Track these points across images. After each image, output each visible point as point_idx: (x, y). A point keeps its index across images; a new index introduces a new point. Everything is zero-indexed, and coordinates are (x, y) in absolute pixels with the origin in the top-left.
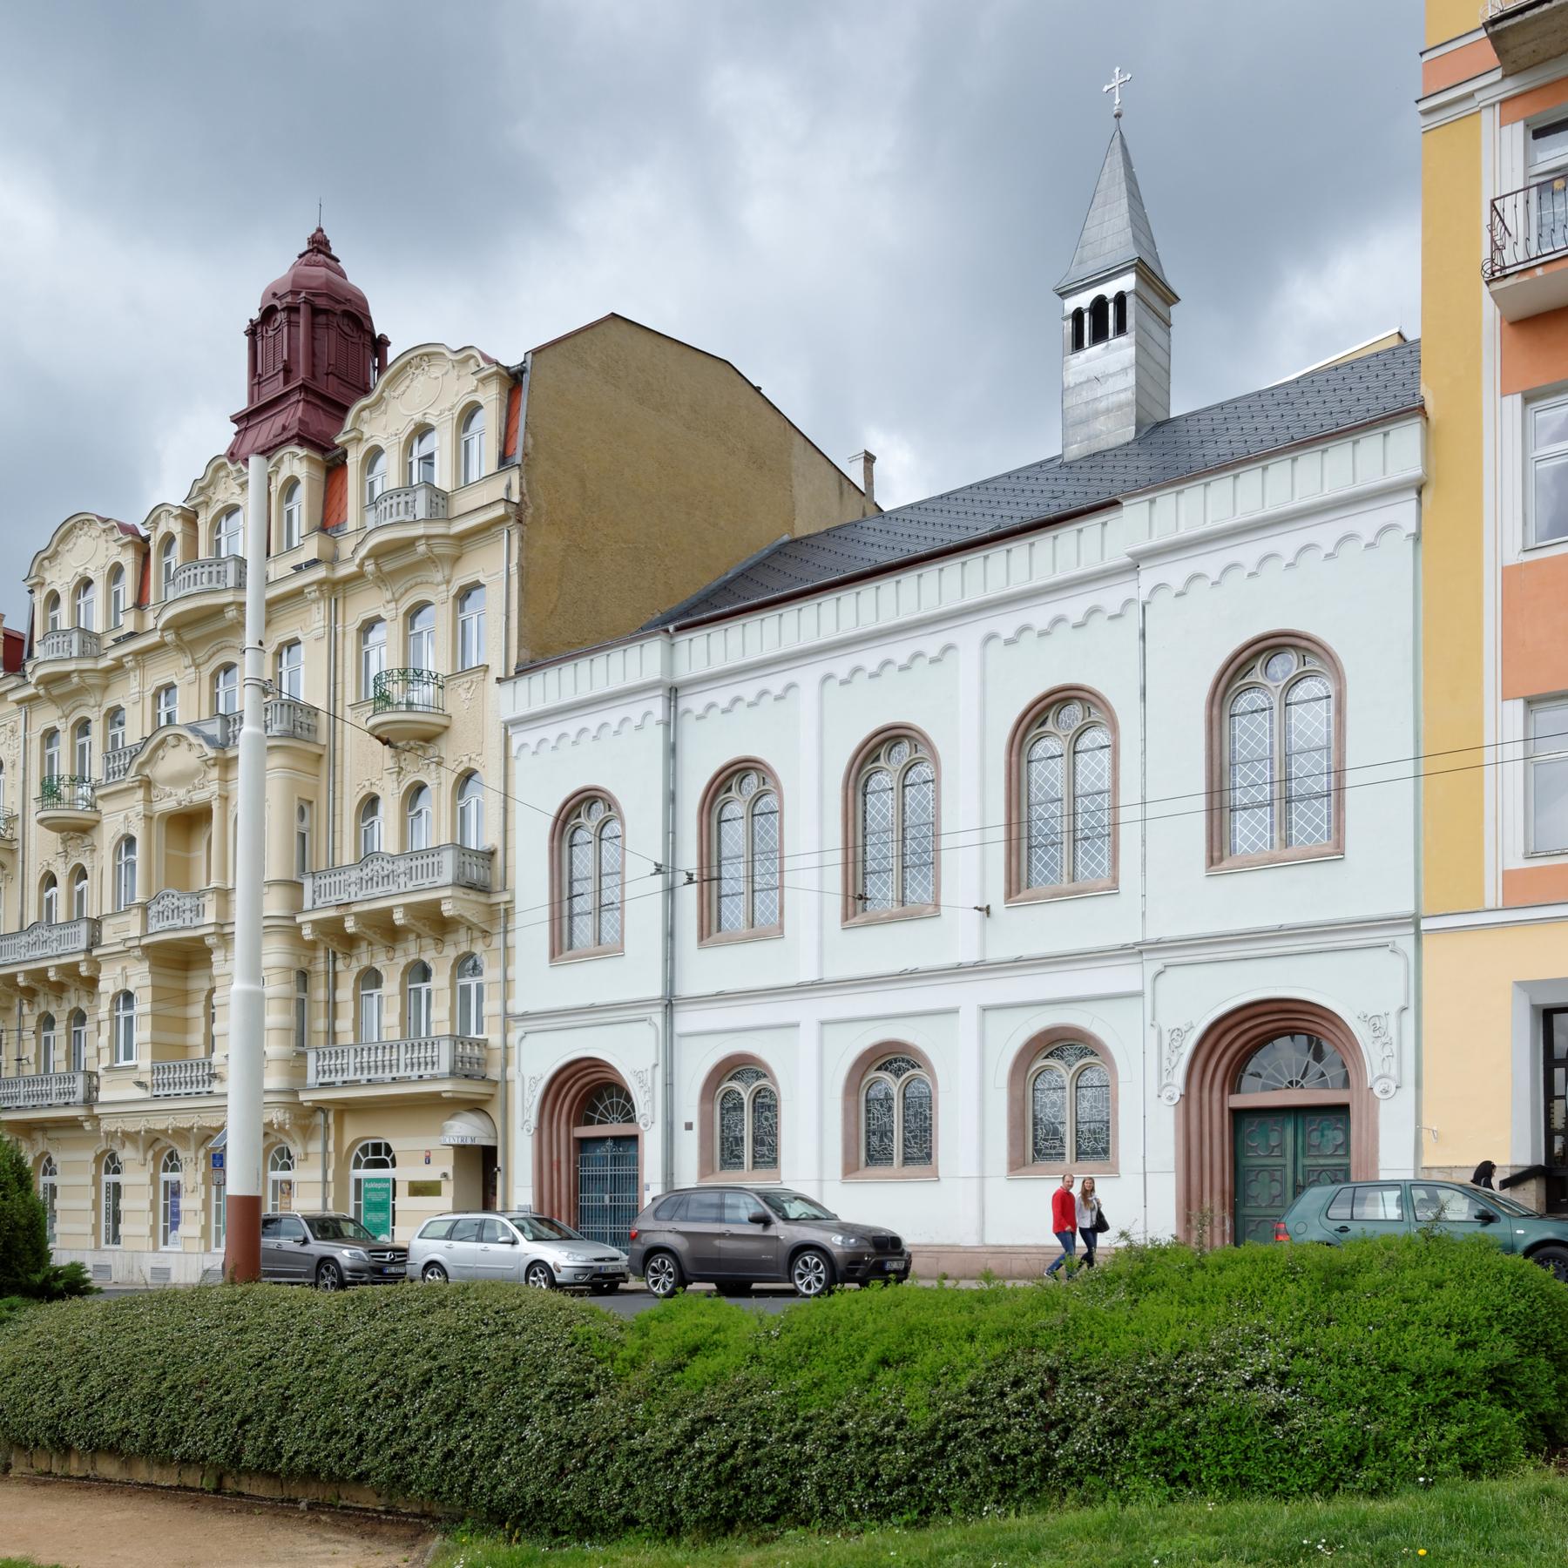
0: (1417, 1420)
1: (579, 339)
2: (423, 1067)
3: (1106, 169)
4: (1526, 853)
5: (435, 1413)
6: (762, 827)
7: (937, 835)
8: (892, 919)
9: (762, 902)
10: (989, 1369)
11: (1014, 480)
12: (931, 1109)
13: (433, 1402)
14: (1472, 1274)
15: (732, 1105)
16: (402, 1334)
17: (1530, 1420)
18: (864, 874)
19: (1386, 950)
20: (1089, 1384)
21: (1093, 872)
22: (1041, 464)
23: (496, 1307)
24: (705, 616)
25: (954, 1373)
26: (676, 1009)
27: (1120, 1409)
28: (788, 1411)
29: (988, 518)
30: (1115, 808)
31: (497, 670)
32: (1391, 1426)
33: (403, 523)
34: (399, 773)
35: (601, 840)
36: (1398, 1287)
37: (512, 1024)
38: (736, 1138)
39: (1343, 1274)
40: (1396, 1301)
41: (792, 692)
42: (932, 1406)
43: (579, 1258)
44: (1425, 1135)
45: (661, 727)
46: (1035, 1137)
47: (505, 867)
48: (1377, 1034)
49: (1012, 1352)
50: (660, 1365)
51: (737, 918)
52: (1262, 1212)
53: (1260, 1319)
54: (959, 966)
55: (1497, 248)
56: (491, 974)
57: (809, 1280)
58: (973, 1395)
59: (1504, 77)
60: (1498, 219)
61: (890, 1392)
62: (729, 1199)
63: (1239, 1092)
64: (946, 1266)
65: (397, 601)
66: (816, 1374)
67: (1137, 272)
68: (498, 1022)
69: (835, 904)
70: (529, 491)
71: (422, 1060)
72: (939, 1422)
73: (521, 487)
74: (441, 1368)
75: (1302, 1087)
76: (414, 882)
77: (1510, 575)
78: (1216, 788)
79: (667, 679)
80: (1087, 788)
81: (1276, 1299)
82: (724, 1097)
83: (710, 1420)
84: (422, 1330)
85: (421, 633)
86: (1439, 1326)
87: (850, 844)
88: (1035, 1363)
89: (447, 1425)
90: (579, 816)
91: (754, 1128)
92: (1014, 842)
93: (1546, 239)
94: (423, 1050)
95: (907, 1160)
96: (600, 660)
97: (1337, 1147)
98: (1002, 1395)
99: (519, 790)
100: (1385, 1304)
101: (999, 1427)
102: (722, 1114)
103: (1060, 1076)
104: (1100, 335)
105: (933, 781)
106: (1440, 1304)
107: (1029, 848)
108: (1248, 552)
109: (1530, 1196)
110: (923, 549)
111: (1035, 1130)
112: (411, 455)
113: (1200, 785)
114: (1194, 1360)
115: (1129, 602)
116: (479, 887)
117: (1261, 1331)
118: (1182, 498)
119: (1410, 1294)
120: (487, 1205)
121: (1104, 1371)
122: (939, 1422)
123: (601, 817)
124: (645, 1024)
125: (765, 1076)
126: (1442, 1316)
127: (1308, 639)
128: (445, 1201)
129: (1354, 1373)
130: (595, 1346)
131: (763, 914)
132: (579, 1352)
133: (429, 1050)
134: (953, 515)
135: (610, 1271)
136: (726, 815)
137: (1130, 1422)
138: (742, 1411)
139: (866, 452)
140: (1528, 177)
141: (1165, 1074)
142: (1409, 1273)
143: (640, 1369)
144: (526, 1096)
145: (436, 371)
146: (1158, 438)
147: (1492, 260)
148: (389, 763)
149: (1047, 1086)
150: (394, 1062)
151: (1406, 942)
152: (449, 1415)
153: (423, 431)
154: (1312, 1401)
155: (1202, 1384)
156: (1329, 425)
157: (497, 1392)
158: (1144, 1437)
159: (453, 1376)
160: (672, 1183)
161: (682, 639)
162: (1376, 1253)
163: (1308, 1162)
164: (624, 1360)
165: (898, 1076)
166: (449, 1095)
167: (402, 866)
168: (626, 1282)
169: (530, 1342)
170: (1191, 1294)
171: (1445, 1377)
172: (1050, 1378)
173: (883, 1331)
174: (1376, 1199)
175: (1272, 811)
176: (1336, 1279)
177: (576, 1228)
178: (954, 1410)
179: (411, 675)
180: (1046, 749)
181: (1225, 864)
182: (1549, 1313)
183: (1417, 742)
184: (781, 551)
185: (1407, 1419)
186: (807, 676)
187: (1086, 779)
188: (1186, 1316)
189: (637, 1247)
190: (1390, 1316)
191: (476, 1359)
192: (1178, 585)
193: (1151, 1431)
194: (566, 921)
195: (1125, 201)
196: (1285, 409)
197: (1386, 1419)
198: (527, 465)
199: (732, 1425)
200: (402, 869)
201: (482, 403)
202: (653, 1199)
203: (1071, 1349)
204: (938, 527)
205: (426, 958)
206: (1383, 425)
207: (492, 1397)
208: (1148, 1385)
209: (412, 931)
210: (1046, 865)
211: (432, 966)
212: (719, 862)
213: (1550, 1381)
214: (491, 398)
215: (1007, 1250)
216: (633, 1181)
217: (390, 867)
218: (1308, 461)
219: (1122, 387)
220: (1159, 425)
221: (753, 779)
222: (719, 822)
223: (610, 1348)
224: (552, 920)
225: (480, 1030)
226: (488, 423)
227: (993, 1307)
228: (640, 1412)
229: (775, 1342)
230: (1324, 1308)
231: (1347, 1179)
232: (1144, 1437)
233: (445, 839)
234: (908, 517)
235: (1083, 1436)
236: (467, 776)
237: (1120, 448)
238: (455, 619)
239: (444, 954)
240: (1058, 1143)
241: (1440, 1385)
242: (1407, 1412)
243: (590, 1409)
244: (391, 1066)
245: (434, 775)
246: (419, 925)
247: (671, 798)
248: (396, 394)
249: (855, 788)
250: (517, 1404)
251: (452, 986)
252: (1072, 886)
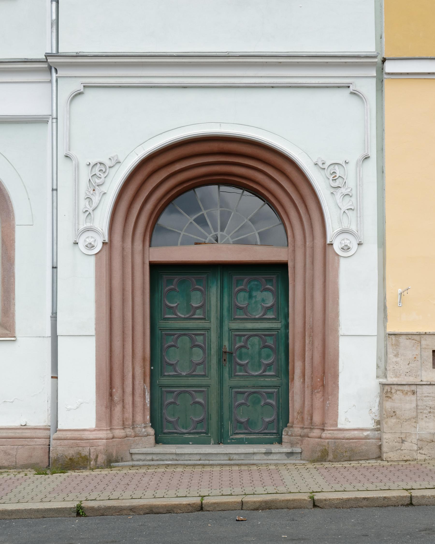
52: (183, 381)
163: (235, 325)
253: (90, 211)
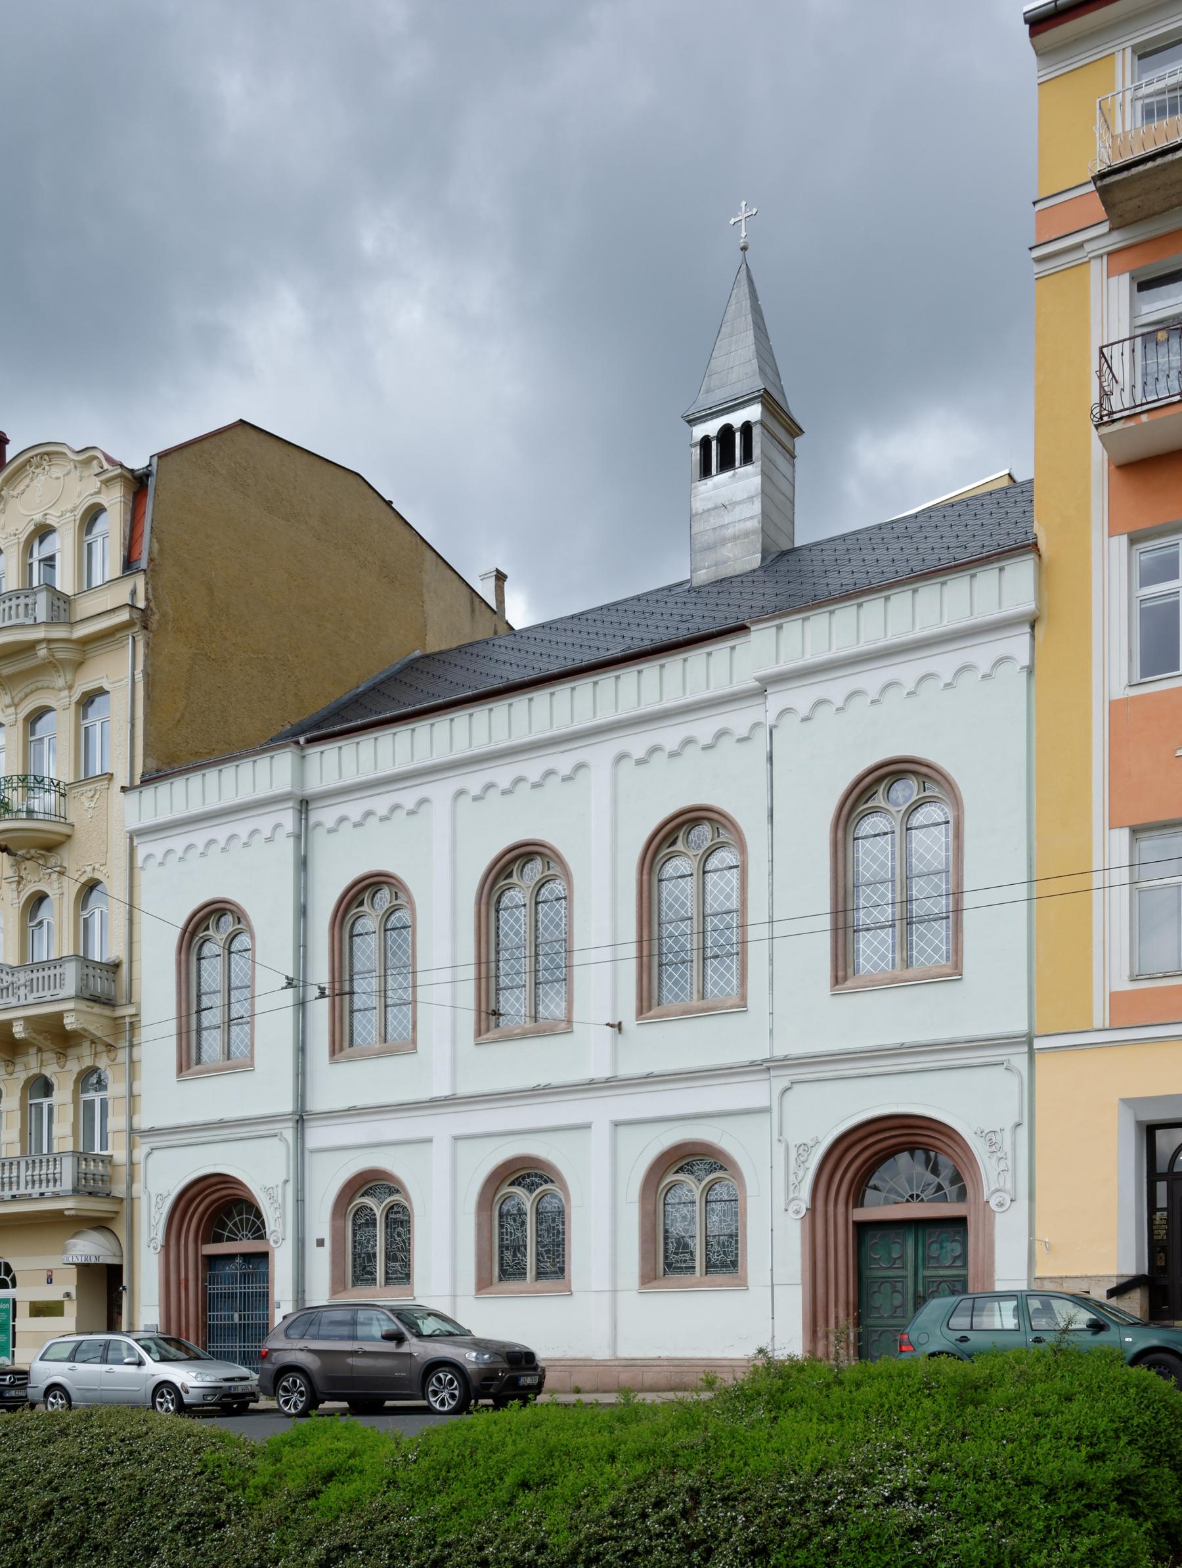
0: (1050, 1532)
1: (206, 444)
2: (44, 1184)
3: (733, 300)
4: (1131, 975)
5: (57, 1546)
6: (394, 941)
7: (569, 951)
8: (525, 1035)
9: (395, 1017)
10: (630, 1491)
11: (643, 603)
12: (563, 1224)
13: (55, 1535)
14: (1099, 1387)
15: (364, 1220)
16: (21, 1465)
17: (1155, 1529)
18: (497, 990)
19: (1002, 1068)
20: (731, 1503)
21: (722, 990)
22: (669, 588)
23: (121, 1434)
24: (336, 728)
25: (596, 1495)
26: (307, 1124)
27: (762, 1528)
28: (427, 1537)
29: (619, 639)
30: (743, 926)
31: (122, 779)
32: (1026, 1539)
33: (22, 626)
34: (19, 883)
35: (230, 953)
36: (1029, 1400)
37: (138, 1139)
38: (368, 1254)
39: (976, 1388)
40: (1028, 1415)
41: (425, 807)
42: (573, 1529)
43: (208, 1379)
44: (1038, 1246)
45: (291, 840)
46: (666, 1250)
47: (131, 980)
48: (993, 1149)
49: (654, 1473)
50: (294, 1493)
51: (370, 1033)
52: (884, 1322)
53: (897, 1435)
54: (592, 1082)
55: (1105, 394)
56: (116, 1088)
57: (443, 1397)
58: (615, 1517)
59: (1111, 230)
60: (1105, 366)
61: (530, 1516)
62: (362, 1315)
63: (862, 1205)
64: (579, 1379)
65: (16, 706)
66: (456, 1498)
67: (763, 405)
68: (123, 1138)
69: (468, 1019)
70: (155, 597)
71: (43, 1177)
72: (581, 1545)
73: (146, 593)
74: (63, 1500)
75: (922, 1200)
76: (35, 995)
77: (1117, 708)
78: (840, 908)
79: (299, 792)
80: (716, 907)
81: (912, 1414)
82: (355, 1215)
83: (345, 1548)
84: (42, 1461)
85: (41, 739)
86: (1070, 1439)
87: (483, 960)
88: (677, 1483)
89: (69, 1559)
90: (207, 928)
91: (387, 1244)
92: (645, 959)
93: (1150, 387)
94: (44, 1168)
95: (540, 1274)
96: (229, 771)
97: (955, 1259)
98: (644, 1516)
99: (144, 900)
100: (1017, 1418)
101: (641, 1549)
102: (354, 1230)
103: (690, 1191)
104: (727, 463)
105: (565, 898)
106: (1070, 1418)
107: (660, 965)
108: (871, 679)
109: (1134, 1304)
110: (554, 668)
111: (666, 1244)
112: (31, 556)
113: (826, 905)
114: (834, 1477)
115: (756, 725)
116: (103, 999)
117: (899, 1446)
118: (808, 624)
119: (1041, 1407)
120: (112, 1325)
121: (746, 1490)
122: (581, 1545)
123: (231, 929)
124: (275, 1140)
125: (398, 1191)
126: (1072, 1429)
127: (928, 766)
128: (68, 1321)
129: (989, 1487)
130: (226, 1473)
131: (395, 1029)
132: (209, 1480)
133: (51, 1167)
134: (584, 635)
135: (240, 1391)
136: (358, 929)
137: (772, 1541)
138: (379, 1538)
139: (497, 570)
140: (1133, 327)
141: (792, 1188)
142: (1039, 1387)
143: (272, 1497)
144: (153, 1213)
145: (57, 471)
146: (783, 566)
147: (1101, 405)
148: (8, 871)
149: (677, 1200)
150: (14, 1180)
151: (1020, 1061)
152: (71, 1549)
153: (43, 532)
154: (949, 1516)
155: (842, 1501)
156: (946, 558)
157: (122, 1524)
158: (785, 1556)
159: (75, 1508)
160: (304, 1300)
161: (314, 751)
162: (1007, 1367)
163: (928, 1273)
164: (256, 1487)
165: (531, 1191)
166: (72, 1212)
167: (22, 977)
168: (257, 1401)
169: (157, 1470)
170: (829, 1411)
171: (1076, 1489)
172: (692, 1498)
173: (523, 1453)
174: (992, 1310)
175: (893, 932)
176: (970, 1393)
177: (204, 1348)
178: (595, 1533)
179: (30, 782)
180: (676, 868)
181: (849, 983)
182: (1172, 1424)
183: (1030, 867)
184: (413, 666)
185: (1040, 1531)
186: (440, 791)
187: (715, 899)
188: (826, 1433)
189: (268, 1366)
190: (1023, 1430)
191: (100, 1489)
192: (804, 710)
193: (792, 1550)
194: (194, 1035)
195: (751, 333)
196: (903, 542)
197: (1021, 1532)
198: (153, 570)
199: (368, 1553)
200: (22, 981)
201: (106, 505)
202: (285, 1317)
203: (713, 1468)
204: (570, 647)
205: (47, 1072)
206: (999, 560)
207: (117, 1529)
208: (789, 1503)
209: (33, 1045)
210: (676, 983)
211: (54, 1080)
212: (351, 976)
213: (1173, 1491)
214: (115, 500)
215: (639, 1362)
216: (263, 1298)
217: (9, 979)
218: (928, 593)
219: (749, 515)
220: (784, 554)
221: (385, 894)
222: (351, 937)
223: (241, 1475)
224: (179, 1034)
225: (104, 1146)
226: (112, 525)
227: (633, 1427)
228: (273, 1539)
229: (413, 1466)
230: (959, 1423)
231: (964, 1290)
232: (785, 1556)
233: (68, 950)
234: (539, 636)
235: (725, 1556)
236: (91, 886)
237: (746, 574)
238: (77, 726)
239: (66, 1068)
240: (688, 1257)
241: (1072, 1498)
242: (1040, 1525)
243: (221, 1539)
244: (11, 1183)
245: (56, 885)
246: (40, 1038)
247: (302, 912)
248: (15, 493)
249: (488, 904)
250: (144, 1535)
251: (75, 1101)
252: (701, 1003)
253: (797, 1183)
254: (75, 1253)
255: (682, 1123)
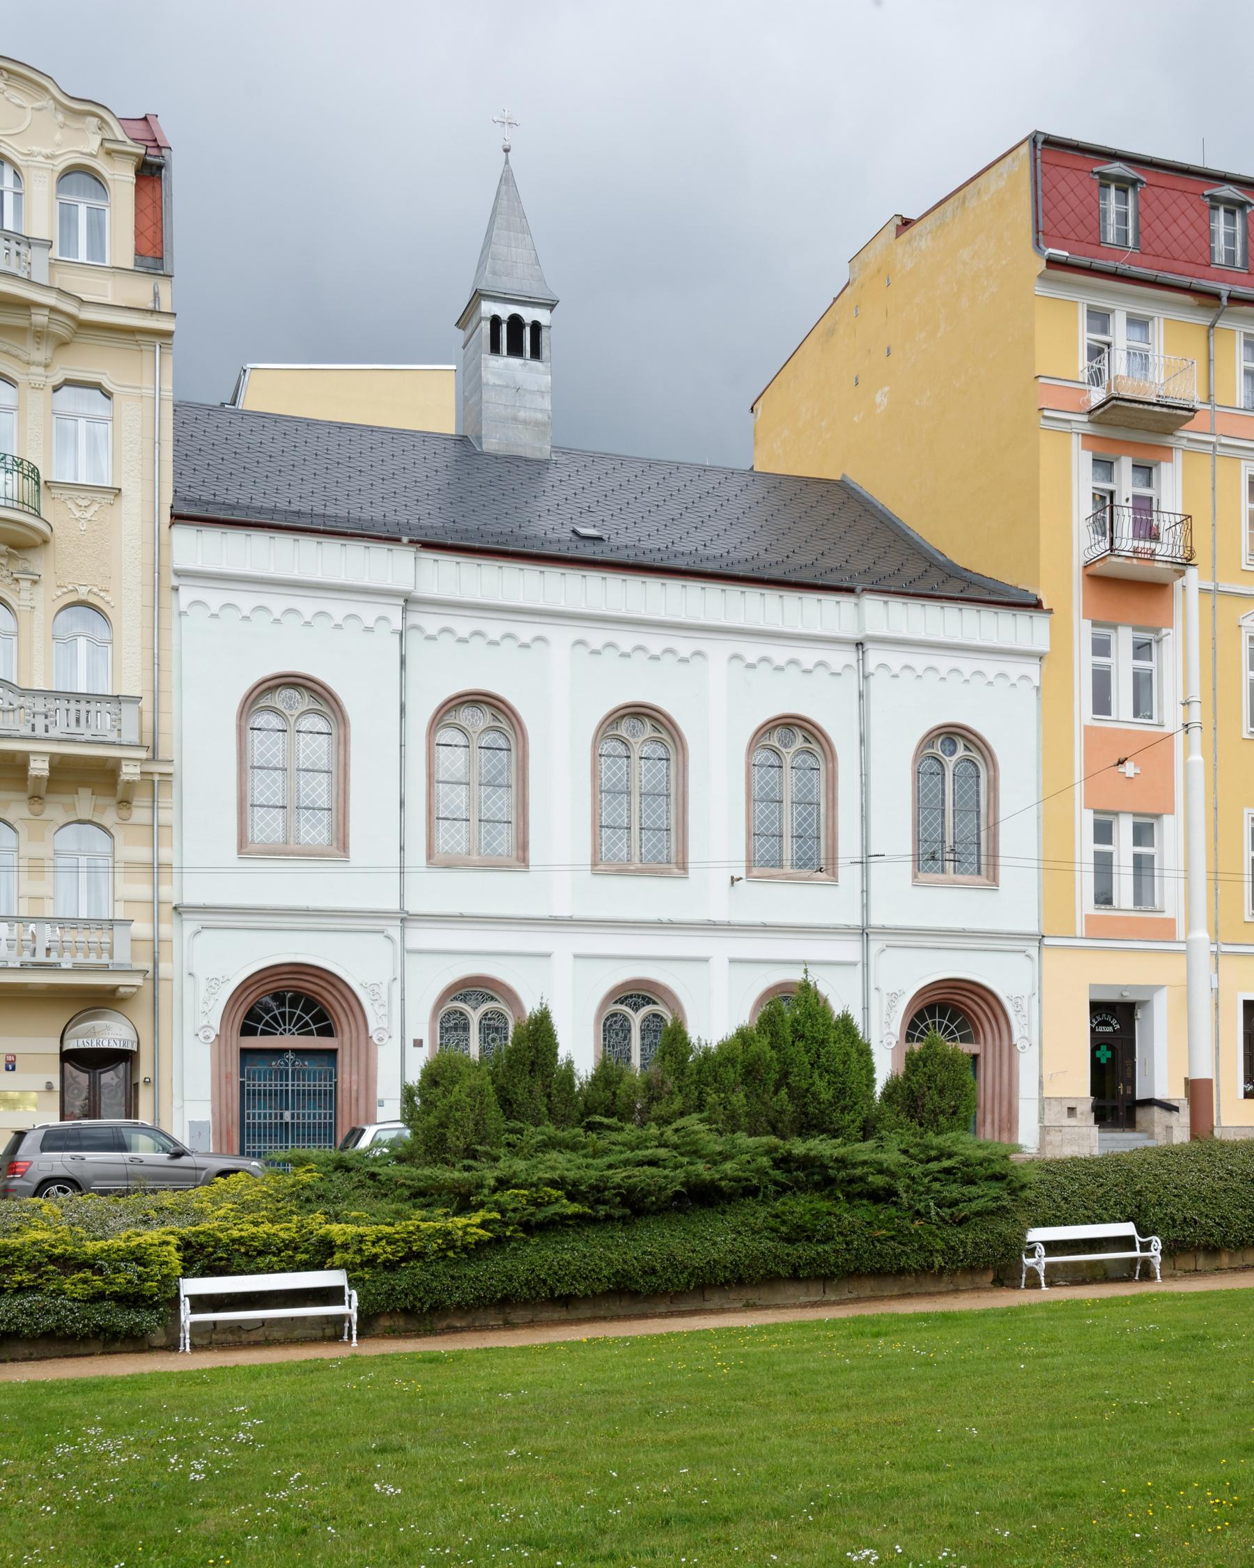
127: (976, 735)
151: (1034, 952)
239: (44, 816)
254: (109, 1036)
255: (782, 966)
